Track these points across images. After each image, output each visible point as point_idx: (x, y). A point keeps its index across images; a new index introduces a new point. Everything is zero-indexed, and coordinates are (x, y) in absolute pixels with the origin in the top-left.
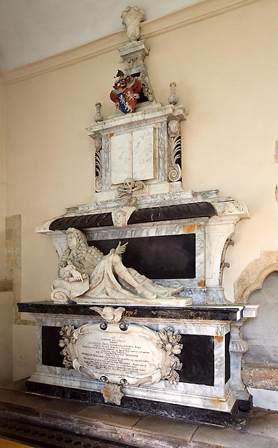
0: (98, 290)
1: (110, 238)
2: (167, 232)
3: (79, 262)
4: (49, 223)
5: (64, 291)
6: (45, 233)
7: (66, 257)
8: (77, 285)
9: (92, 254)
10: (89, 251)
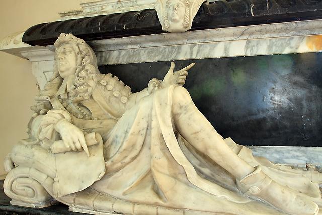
0: (129, 177)
1: (144, 58)
2: (270, 47)
3: (80, 104)
4: (22, 35)
5: (33, 172)
6: (15, 52)
7: (50, 92)
8: (71, 161)
9: (109, 87)
10: (103, 82)
